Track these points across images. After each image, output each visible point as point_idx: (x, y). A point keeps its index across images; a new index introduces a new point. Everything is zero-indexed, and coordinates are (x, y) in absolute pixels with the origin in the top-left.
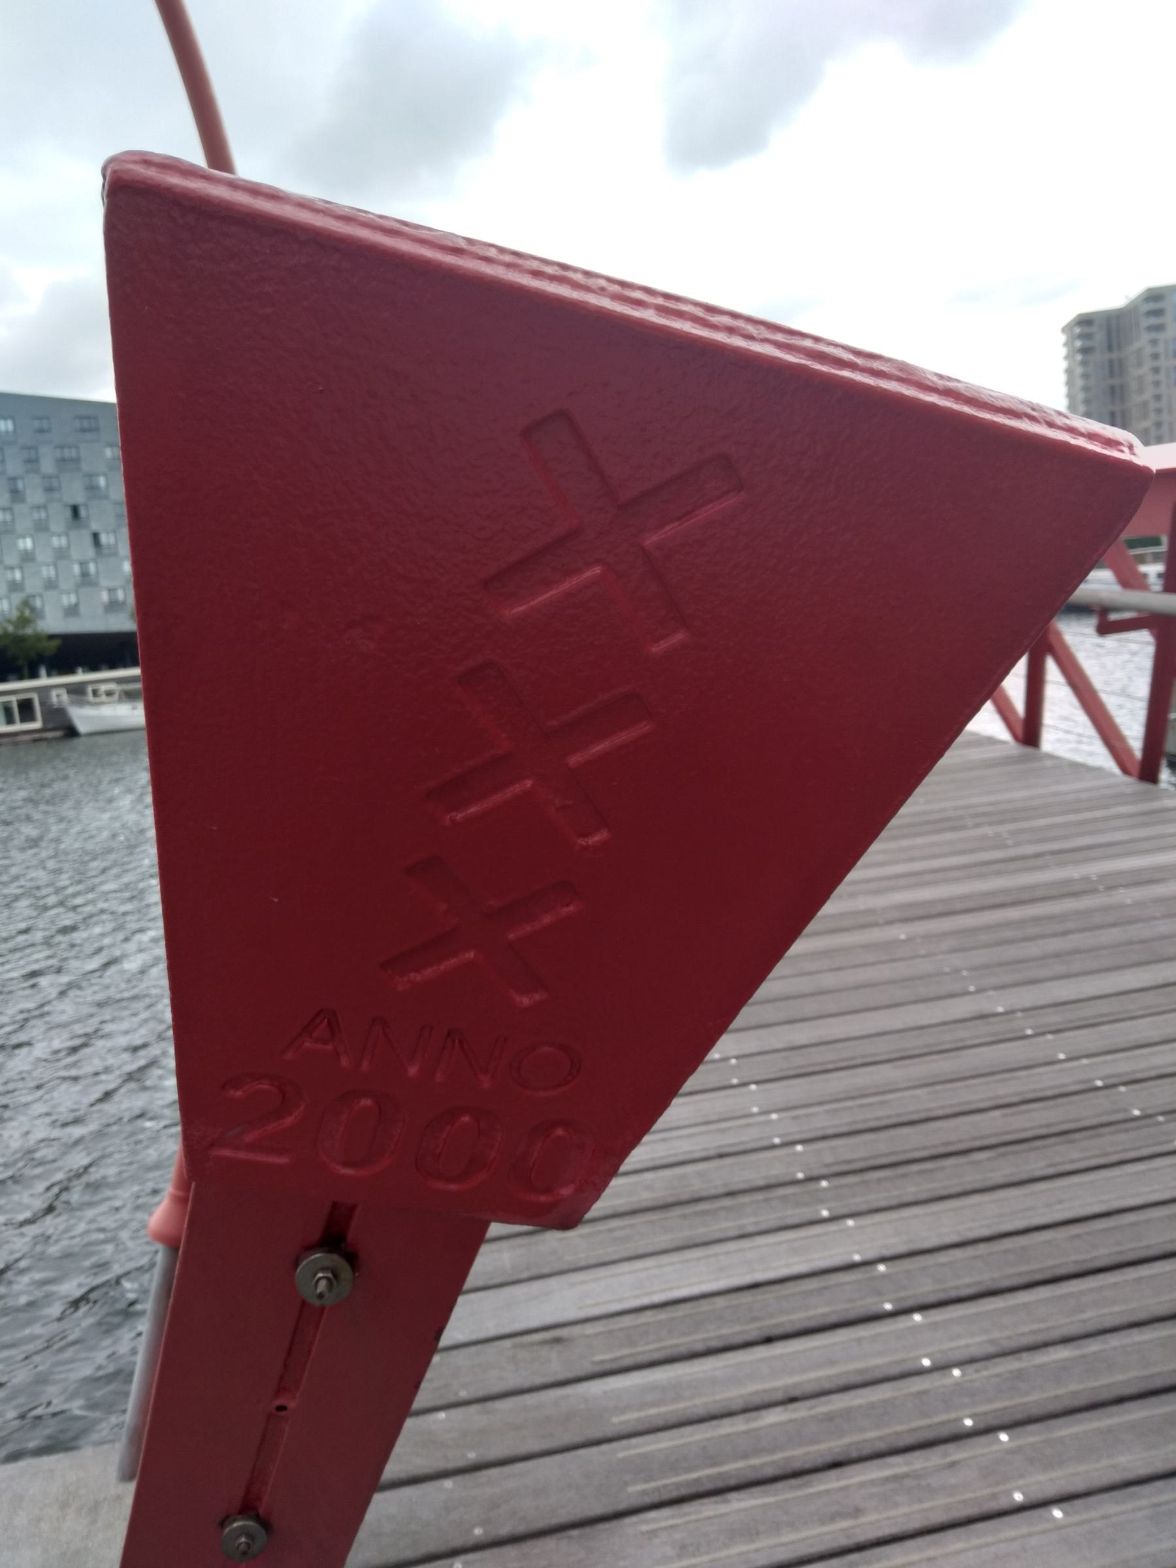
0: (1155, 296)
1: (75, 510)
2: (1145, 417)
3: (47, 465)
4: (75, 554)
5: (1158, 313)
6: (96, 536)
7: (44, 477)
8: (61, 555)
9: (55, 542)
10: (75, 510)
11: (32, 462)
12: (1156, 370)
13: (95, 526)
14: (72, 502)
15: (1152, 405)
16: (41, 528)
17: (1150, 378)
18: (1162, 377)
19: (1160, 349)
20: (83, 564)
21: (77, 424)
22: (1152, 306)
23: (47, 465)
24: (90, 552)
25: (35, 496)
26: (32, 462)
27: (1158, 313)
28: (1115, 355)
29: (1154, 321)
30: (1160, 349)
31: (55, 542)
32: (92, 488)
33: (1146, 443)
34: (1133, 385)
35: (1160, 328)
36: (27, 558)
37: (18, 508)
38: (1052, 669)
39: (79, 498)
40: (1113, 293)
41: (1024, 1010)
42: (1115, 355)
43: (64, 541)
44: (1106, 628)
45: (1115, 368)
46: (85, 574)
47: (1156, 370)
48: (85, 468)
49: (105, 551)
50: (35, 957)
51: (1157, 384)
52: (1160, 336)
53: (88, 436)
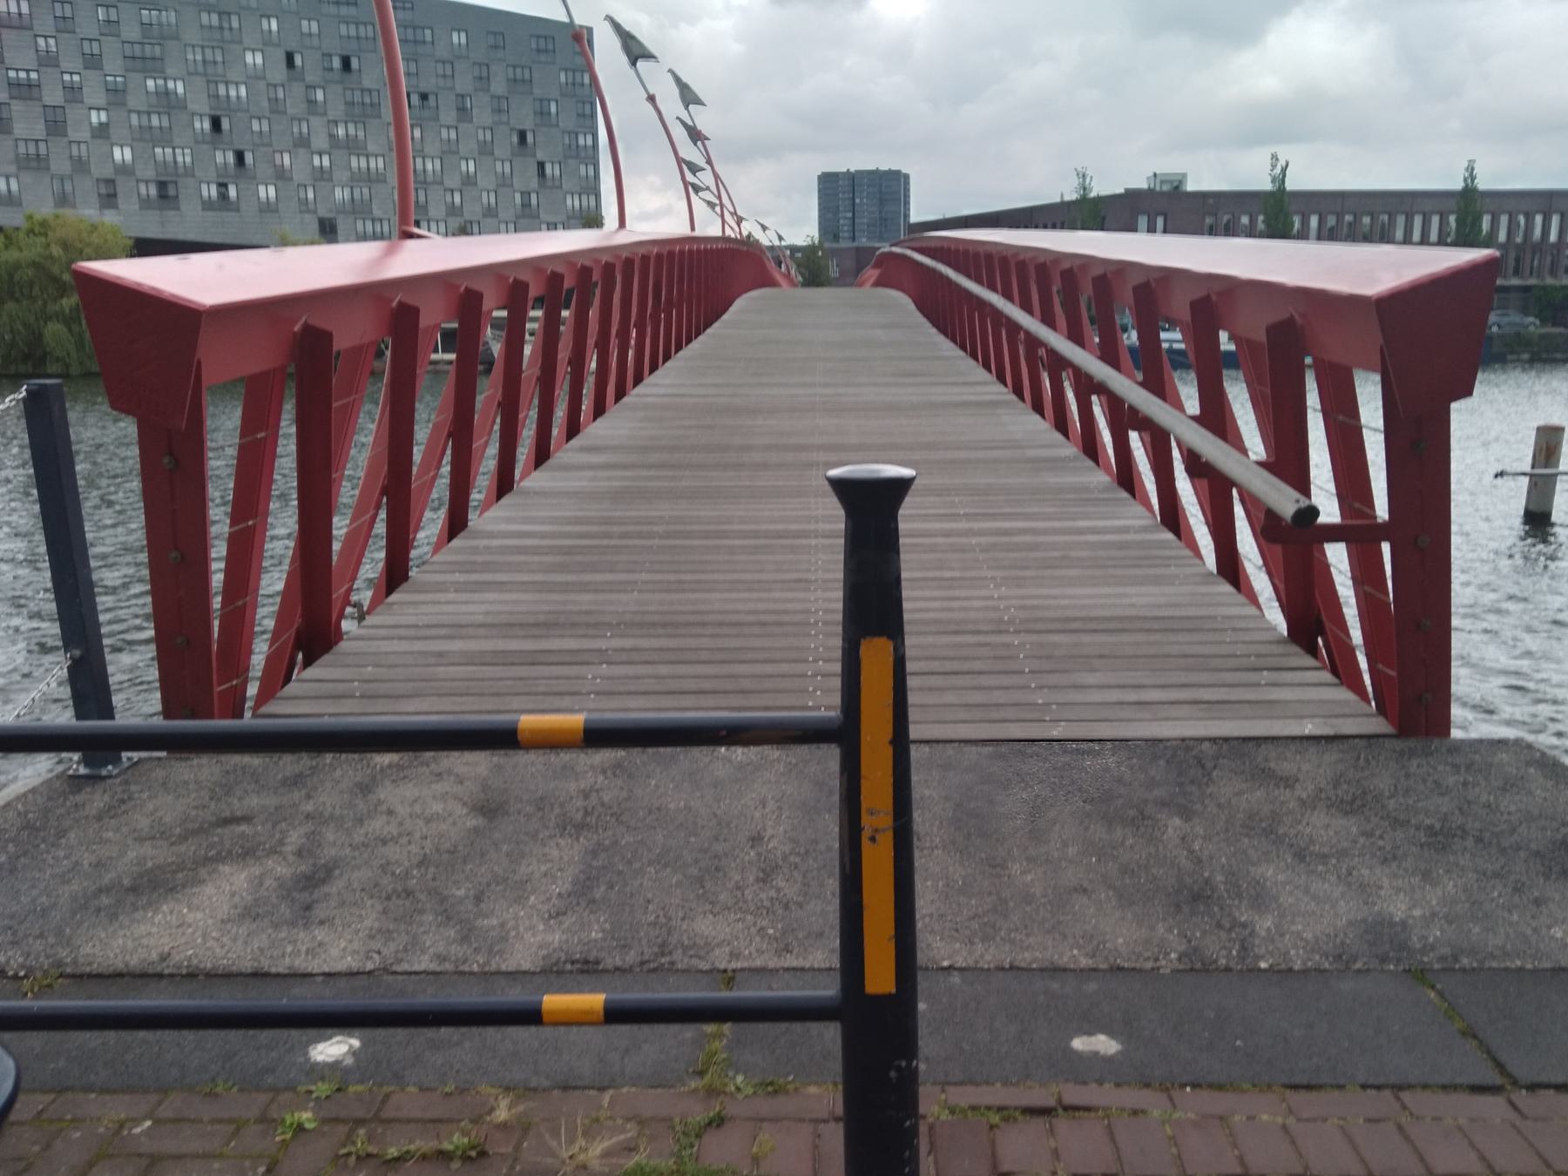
1: (522, 136)
3: (499, 86)
4: (518, 183)
6: (541, 166)
7: (493, 97)
8: (504, 182)
9: (94, 117)
10: (522, 136)
11: (483, 81)
13: (540, 156)
14: (521, 127)
16: (485, 150)
20: (526, 194)
23: (499, 86)
24: (534, 183)
25: (482, 114)
26: (483, 81)
31: (94, 117)
32: (543, 114)
33: (580, 38)
36: (469, 181)
37: (463, 127)
39: (528, 125)
41: (353, 697)
43: (103, 117)
46: (526, 205)
48: (537, 91)
49: (549, 183)
50: (483, 608)
53: (543, 58)
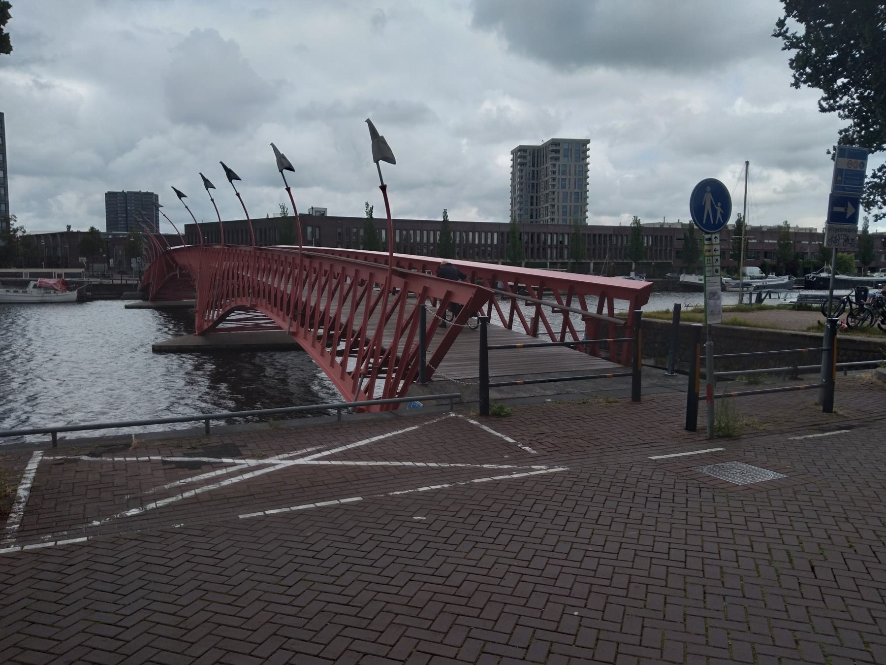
0: (555, 143)
2: (547, 201)
5: (557, 151)
12: (554, 179)
15: (550, 182)
17: (550, 182)
18: (556, 182)
19: (556, 169)
21: (38, 401)
22: (554, 148)
27: (557, 151)
28: (535, 169)
29: (554, 155)
30: (556, 169)
34: (543, 211)
35: (557, 159)
38: (493, 307)
40: (537, 140)
42: (535, 169)
44: (527, 304)
45: (535, 175)
47: (554, 179)
49: (59, 446)
51: (554, 186)
52: (557, 163)
